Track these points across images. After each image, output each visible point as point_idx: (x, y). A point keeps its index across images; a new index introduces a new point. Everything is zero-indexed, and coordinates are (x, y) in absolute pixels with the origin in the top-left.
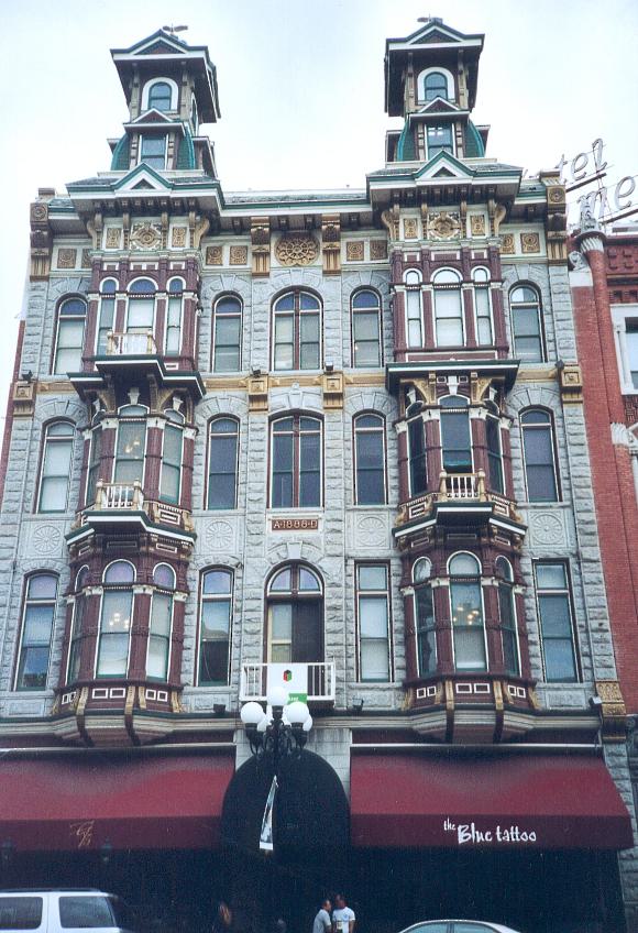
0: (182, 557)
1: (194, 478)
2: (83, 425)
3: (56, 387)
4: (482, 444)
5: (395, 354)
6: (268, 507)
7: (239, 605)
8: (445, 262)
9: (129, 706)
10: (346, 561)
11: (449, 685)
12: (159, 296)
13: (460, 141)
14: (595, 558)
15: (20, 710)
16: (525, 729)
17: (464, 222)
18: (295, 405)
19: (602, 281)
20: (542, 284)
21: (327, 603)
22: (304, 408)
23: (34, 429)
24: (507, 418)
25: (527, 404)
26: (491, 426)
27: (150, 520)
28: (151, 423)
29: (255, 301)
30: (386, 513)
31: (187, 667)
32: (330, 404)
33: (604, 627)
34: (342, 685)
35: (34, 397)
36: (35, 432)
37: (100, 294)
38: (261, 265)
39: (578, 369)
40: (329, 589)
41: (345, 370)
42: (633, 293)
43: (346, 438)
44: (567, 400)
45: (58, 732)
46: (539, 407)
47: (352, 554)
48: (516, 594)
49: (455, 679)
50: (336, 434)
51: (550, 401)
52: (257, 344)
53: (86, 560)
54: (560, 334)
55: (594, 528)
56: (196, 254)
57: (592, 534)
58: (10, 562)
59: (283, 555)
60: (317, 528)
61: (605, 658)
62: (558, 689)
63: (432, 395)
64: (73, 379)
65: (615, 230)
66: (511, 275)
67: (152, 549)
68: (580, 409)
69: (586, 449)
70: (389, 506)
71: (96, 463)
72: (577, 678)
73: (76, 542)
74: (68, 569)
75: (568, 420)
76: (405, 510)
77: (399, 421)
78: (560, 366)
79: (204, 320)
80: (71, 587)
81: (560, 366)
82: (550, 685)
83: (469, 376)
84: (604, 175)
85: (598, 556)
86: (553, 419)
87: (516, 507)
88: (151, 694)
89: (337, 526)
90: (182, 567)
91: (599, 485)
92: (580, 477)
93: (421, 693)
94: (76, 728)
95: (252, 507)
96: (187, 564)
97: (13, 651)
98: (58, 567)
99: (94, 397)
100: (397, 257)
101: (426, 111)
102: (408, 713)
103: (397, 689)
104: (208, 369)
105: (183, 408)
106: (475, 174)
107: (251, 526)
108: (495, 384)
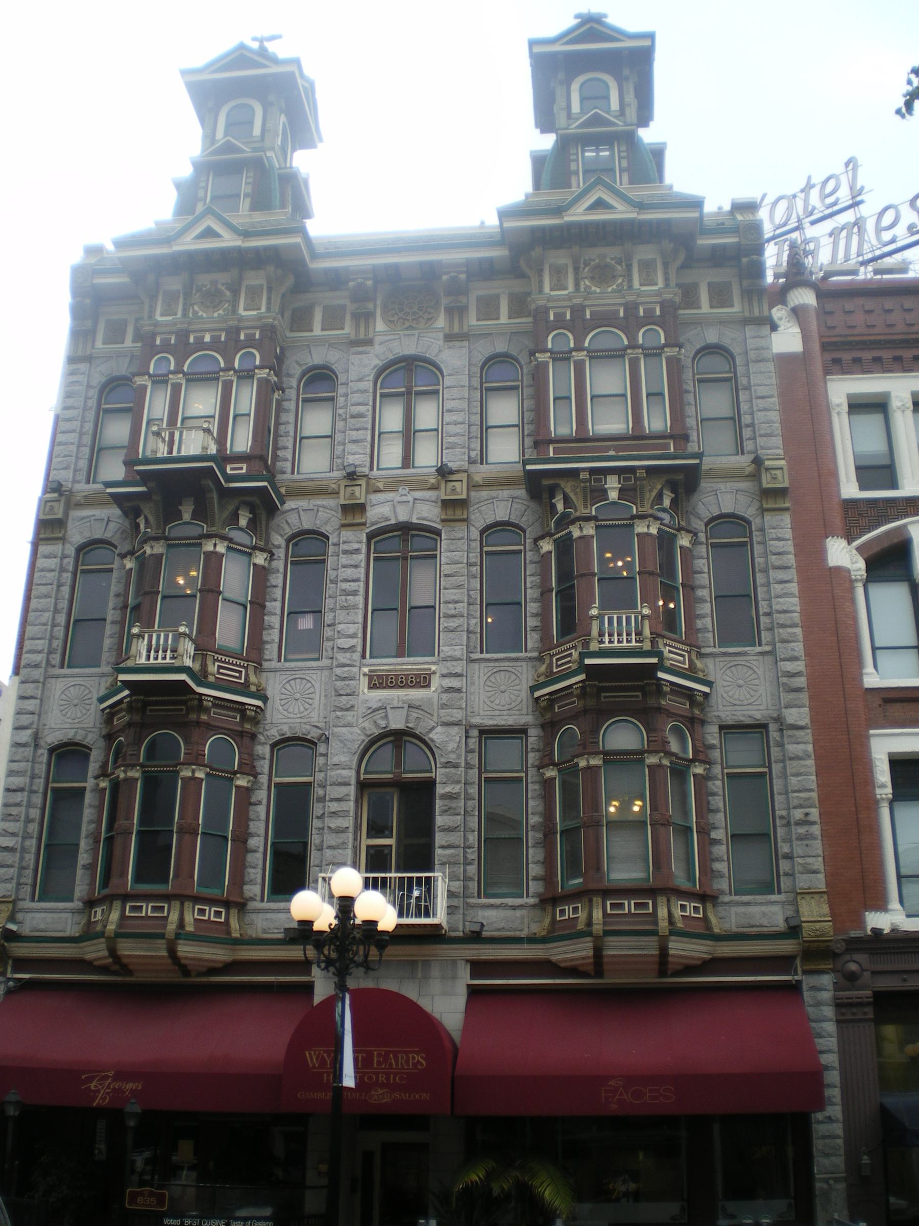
0: (247, 726)
1: (266, 618)
2: (124, 551)
3: (90, 501)
4: (650, 568)
5: (536, 444)
6: (364, 657)
7: (321, 792)
8: (605, 319)
9: (172, 927)
10: (467, 732)
11: (597, 900)
12: (223, 376)
13: (624, 163)
14: (802, 723)
15: (42, 926)
16: (699, 959)
17: (629, 267)
18: (403, 517)
19: (816, 347)
20: (736, 350)
21: (440, 790)
22: (415, 521)
23: (64, 556)
24: (688, 531)
25: (716, 512)
26: (666, 541)
27: (201, 677)
28: (208, 547)
29: (353, 375)
30: (524, 664)
31: (252, 876)
32: (450, 515)
33: (811, 818)
34: (455, 902)
35: (66, 514)
36: (66, 560)
37: (150, 376)
38: (362, 330)
39: (782, 463)
40: (443, 770)
41: (473, 469)
42: (917, 358)
43: (472, 560)
44: (769, 506)
45: (88, 957)
46: (732, 516)
47: (476, 720)
48: (694, 775)
49: (606, 893)
50: (457, 555)
51: (747, 508)
52: (355, 435)
53: (122, 730)
54: (759, 416)
55: (801, 682)
56: (274, 319)
57: (798, 690)
58: (29, 732)
59: (383, 723)
60: (428, 686)
61: (810, 860)
62: (748, 904)
63: (585, 501)
64: (109, 490)
65: (876, 272)
66: (695, 338)
67: (204, 717)
68: (786, 519)
69: (792, 574)
70: (529, 655)
71: (137, 601)
72: (768, 887)
73: (111, 706)
74: (101, 743)
75: (772, 533)
76: (547, 661)
77: (542, 537)
78: (758, 462)
79: (286, 404)
80: (104, 766)
81: (758, 462)
82: (737, 898)
83: (635, 474)
84: (861, 202)
85: (805, 721)
86: (751, 532)
87: (700, 655)
88: (202, 912)
89: (455, 683)
90: (246, 740)
91: (810, 623)
92: (785, 612)
93: (562, 912)
94: (106, 953)
95: (342, 658)
96: (253, 736)
97: (33, 850)
98: (89, 740)
99: (137, 513)
100: (540, 314)
101: (580, 126)
102: (543, 940)
103: (534, 906)
104: (289, 470)
105: (253, 525)
106: (641, 206)
107: (339, 684)
108: (673, 487)
